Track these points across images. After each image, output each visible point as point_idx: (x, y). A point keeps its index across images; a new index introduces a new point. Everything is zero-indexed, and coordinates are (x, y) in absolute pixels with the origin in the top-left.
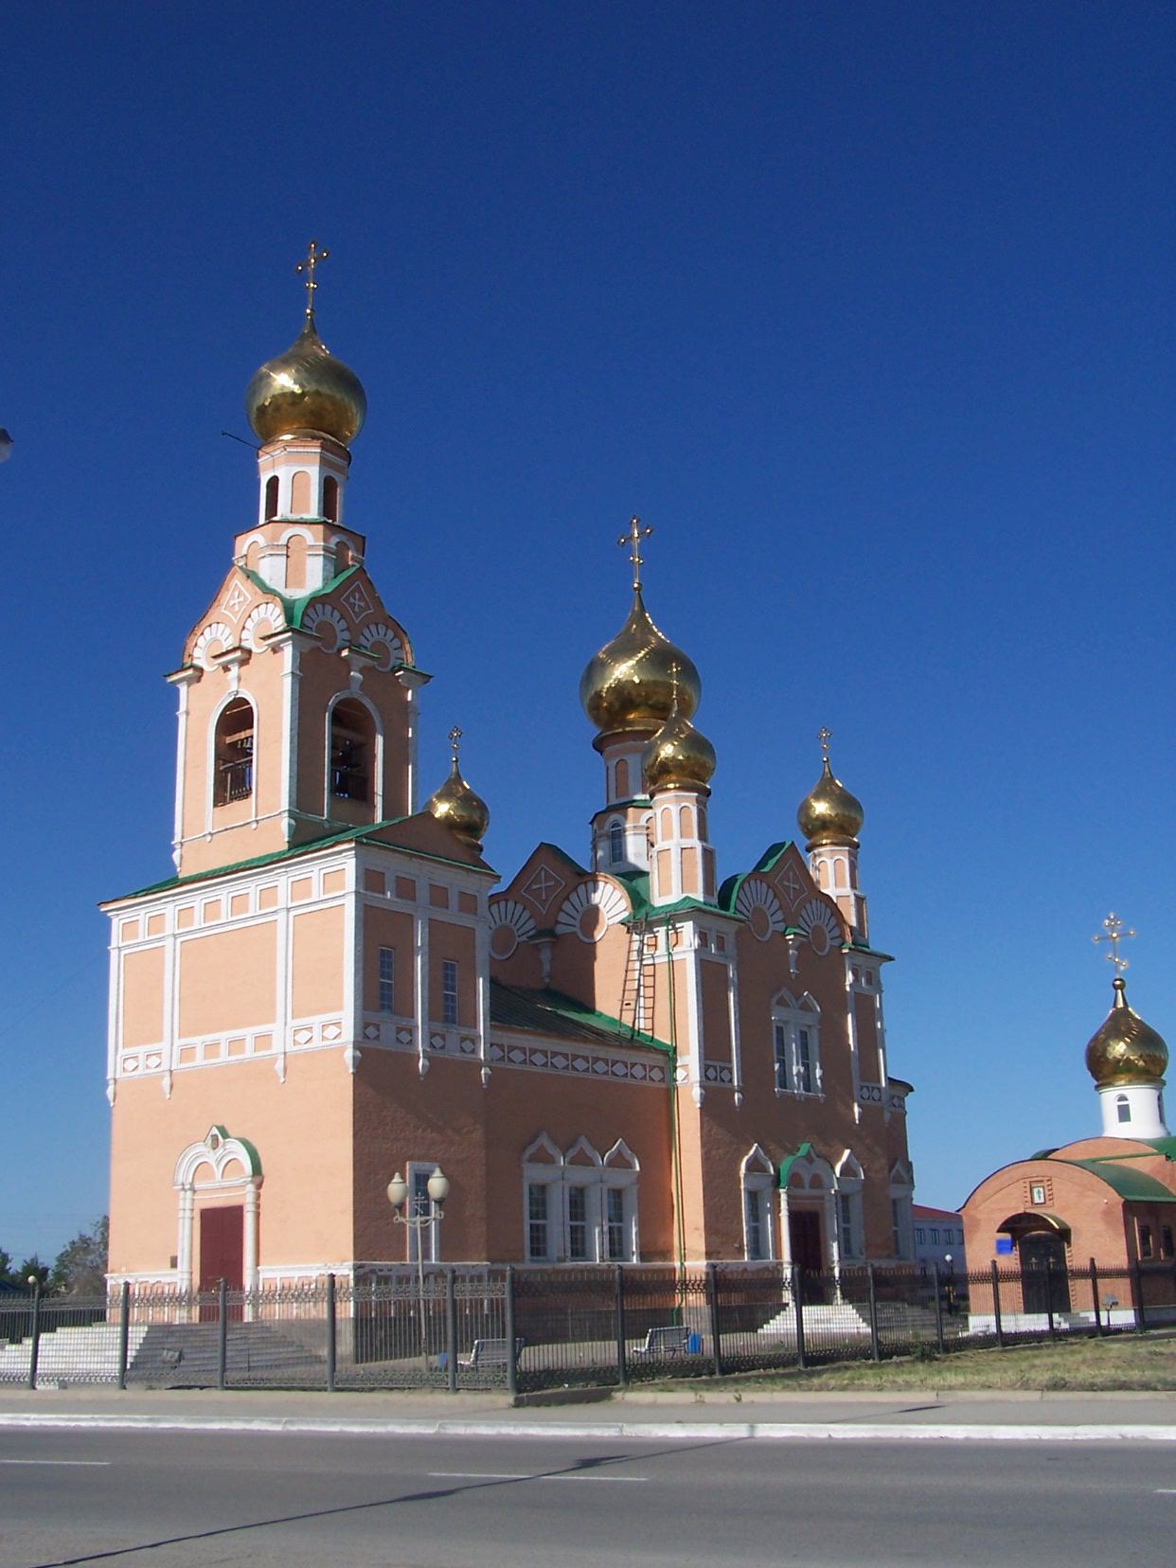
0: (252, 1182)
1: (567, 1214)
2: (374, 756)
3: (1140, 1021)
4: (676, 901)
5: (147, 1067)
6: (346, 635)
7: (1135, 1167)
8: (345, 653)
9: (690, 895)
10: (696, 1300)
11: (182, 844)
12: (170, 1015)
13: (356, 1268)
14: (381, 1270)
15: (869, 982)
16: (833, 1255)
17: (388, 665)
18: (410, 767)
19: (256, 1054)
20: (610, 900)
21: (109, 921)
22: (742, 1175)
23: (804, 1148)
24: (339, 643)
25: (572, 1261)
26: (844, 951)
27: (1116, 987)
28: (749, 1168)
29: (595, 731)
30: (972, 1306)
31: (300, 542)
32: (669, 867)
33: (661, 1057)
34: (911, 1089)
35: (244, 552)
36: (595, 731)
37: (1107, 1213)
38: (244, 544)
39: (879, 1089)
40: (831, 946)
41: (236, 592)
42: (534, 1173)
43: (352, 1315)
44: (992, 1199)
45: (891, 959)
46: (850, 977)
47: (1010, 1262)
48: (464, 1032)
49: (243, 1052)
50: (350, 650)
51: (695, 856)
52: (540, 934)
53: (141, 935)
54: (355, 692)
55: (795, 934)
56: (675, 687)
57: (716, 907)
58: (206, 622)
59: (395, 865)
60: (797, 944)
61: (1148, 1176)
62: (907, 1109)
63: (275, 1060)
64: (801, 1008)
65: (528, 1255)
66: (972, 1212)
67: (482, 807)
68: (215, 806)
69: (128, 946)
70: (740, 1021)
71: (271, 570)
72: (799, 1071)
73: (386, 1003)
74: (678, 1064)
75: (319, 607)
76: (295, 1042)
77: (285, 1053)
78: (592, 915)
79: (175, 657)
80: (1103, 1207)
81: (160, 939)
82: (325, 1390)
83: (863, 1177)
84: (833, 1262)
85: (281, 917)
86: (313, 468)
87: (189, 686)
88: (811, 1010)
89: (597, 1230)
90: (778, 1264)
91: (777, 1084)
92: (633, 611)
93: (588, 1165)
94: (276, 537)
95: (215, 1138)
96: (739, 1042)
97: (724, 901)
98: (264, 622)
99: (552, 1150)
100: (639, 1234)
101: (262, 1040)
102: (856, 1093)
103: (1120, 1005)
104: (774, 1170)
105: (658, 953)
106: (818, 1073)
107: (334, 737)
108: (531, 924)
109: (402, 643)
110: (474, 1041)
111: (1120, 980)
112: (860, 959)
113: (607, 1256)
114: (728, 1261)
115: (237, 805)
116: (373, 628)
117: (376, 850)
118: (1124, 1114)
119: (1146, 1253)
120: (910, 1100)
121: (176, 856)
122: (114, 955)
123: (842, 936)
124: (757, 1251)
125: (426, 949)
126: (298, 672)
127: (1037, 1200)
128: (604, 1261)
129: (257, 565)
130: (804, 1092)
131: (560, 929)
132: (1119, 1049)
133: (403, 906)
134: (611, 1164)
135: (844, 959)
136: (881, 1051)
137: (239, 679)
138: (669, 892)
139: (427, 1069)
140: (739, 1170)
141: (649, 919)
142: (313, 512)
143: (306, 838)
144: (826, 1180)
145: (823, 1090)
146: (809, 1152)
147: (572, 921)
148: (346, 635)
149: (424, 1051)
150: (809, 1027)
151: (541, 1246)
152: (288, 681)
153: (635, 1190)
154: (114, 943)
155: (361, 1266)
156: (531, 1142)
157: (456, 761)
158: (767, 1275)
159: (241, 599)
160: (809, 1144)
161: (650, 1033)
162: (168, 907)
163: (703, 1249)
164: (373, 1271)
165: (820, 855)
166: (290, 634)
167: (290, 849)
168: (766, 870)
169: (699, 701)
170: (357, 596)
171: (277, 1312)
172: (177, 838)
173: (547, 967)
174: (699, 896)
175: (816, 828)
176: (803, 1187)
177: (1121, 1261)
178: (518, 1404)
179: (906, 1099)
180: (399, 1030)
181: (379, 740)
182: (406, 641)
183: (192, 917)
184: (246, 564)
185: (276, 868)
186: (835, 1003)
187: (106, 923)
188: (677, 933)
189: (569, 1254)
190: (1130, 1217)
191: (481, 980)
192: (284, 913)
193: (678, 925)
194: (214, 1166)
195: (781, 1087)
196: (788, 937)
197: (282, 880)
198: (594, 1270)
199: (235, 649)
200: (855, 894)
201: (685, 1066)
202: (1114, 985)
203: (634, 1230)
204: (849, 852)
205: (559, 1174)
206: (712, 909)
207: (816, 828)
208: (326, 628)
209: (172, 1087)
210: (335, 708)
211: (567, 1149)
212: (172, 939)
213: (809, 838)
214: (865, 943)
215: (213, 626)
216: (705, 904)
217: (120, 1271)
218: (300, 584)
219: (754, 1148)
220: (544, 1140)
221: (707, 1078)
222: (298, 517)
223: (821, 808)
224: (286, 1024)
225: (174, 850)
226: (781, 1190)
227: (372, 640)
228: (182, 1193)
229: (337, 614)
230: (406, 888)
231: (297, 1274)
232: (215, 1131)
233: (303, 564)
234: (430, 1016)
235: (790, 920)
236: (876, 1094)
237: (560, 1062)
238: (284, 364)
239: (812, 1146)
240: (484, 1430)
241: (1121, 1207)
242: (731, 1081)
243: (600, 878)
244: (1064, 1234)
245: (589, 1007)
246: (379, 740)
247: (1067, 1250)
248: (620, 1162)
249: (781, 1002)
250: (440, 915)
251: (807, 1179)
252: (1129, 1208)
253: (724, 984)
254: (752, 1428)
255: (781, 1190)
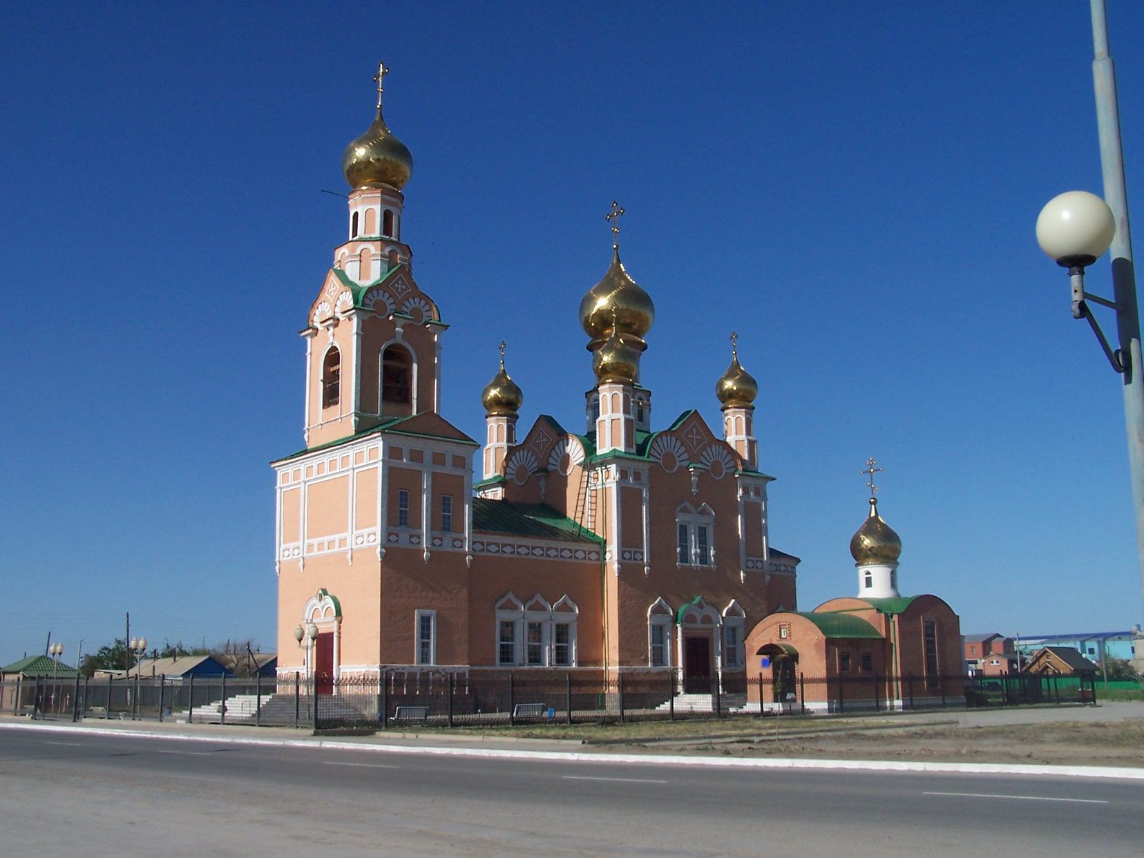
0: (336, 620)
1: (526, 638)
2: (411, 376)
3: (884, 524)
4: (607, 452)
5: (369, 542)
6: (393, 307)
7: (859, 616)
8: (391, 318)
9: (617, 448)
10: (614, 690)
11: (308, 429)
12: (303, 528)
13: (381, 668)
14: (397, 669)
15: (757, 493)
16: (717, 664)
17: (422, 320)
18: (436, 381)
19: (340, 549)
20: (575, 450)
21: (276, 472)
22: (648, 616)
23: (698, 599)
24: (388, 311)
25: (529, 665)
26: (737, 476)
27: (871, 503)
28: (653, 612)
29: (589, 339)
30: (749, 698)
31: (368, 253)
32: (604, 433)
33: (597, 546)
34: (799, 561)
35: (339, 259)
36: (589, 339)
37: (817, 645)
38: (342, 252)
39: (762, 562)
40: (726, 473)
41: (333, 282)
42: (503, 616)
43: (379, 693)
44: (761, 634)
45: (774, 479)
46: (740, 492)
47: (768, 673)
48: (455, 536)
49: (323, 550)
50: (394, 316)
51: (620, 423)
52: (539, 471)
53: (338, 469)
54: (399, 340)
55: (694, 468)
56: (614, 319)
57: (634, 454)
58: (319, 301)
59: (407, 443)
60: (698, 473)
61: (865, 622)
62: (797, 574)
63: (347, 553)
64: (699, 513)
65: (498, 661)
66: (751, 642)
67: (518, 391)
68: (324, 408)
69: (311, 480)
70: (650, 524)
71: (352, 271)
72: (696, 552)
73: (403, 521)
74: (607, 550)
75: (375, 292)
76: (356, 544)
77: (352, 549)
78: (566, 458)
79: (305, 323)
80: (815, 641)
81: (299, 483)
82: (254, 725)
83: (745, 616)
84: (718, 668)
85: (302, 485)
86: (377, 206)
87: (312, 338)
88: (709, 514)
89: (547, 648)
90: (674, 669)
91: (678, 560)
92: (613, 263)
93: (515, 609)
94: (353, 250)
95: (320, 595)
96: (649, 536)
97: (641, 450)
98: (344, 302)
99: (543, 602)
100: (578, 650)
101: (342, 542)
102: (742, 568)
103: (873, 514)
104: (673, 613)
105: (598, 483)
106: (712, 552)
107: (385, 368)
108: (535, 465)
109: (431, 306)
110: (462, 541)
111: (874, 499)
112: (748, 481)
113: (554, 662)
114: (635, 667)
115: (332, 408)
116: (411, 301)
117: (395, 436)
118: (869, 583)
119: (843, 668)
120: (798, 568)
121: (306, 436)
122: (278, 491)
123: (736, 466)
124: (659, 658)
125: (430, 490)
126: (361, 333)
127: (783, 636)
128: (551, 666)
129: (345, 267)
130: (700, 565)
131: (550, 468)
132: (867, 542)
133: (416, 466)
134: (558, 609)
135: (737, 482)
136: (764, 538)
137: (334, 335)
138: (604, 446)
139: (428, 558)
140: (647, 612)
141: (592, 463)
142: (377, 233)
143: (363, 429)
144: (714, 619)
145: (716, 563)
146: (700, 602)
147: (707, 463)
148: (393, 307)
149: (427, 548)
150: (708, 524)
151: (509, 656)
152: (355, 337)
153: (575, 624)
154: (278, 486)
155: (384, 667)
156: (503, 596)
157: (503, 363)
158: (665, 677)
159: (335, 288)
160: (700, 597)
161: (593, 531)
162: (301, 465)
163: (618, 660)
164: (393, 670)
165: (727, 415)
166: (354, 311)
167: (356, 434)
168: (674, 429)
169: (654, 320)
170: (400, 282)
171: (348, 690)
172: (307, 426)
173: (543, 491)
174: (622, 448)
175: (726, 397)
176: (696, 622)
177: (822, 673)
178: (316, 734)
179: (797, 567)
180: (411, 536)
181: (415, 366)
182: (433, 306)
183: (323, 468)
184: (340, 266)
185: (348, 446)
186: (727, 508)
187: (274, 474)
188: (608, 471)
189: (527, 661)
190: (831, 647)
191: (467, 506)
192: (351, 471)
193: (608, 466)
194: (321, 609)
195: (681, 562)
196: (690, 470)
197: (350, 451)
198: (431, 667)
199: (330, 319)
200: (748, 439)
201: (610, 551)
202: (870, 502)
203: (574, 648)
204: (746, 413)
205: (521, 615)
206: (633, 457)
207: (726, 397)
208: (380, 306)
209: (304, 566)
210: (385, 350)
211: (526, 602)
212: (352, 470)
213: (723, 402)
214: (755, 470)
215: (323, 303)
216: (625, 453)
217: (282, 666)
218: (368, 278)
219: (658, 600)
220: (510, 596)
221: (624, 558)
222: (368, 237)
223: (729, 384)
224: (352, 533)
225: (305, 433)
226: (678, 625)
227: (410, 307)
228: (307, 625)
229: (387, 295)
230: (416, 456)
231: (356, 670)
232: (320, 592)
233: (369, 265)
234: (433, 527)
235: (692, 459)
236: (759, 565)
237: (523, 551)
238: (360, 144)
239: (702, 598)
240: (300, 744)
241: (824, 641)
242: (642, 559)
243: (570, 437)
244: (794, 657)
245: (561, 514)
246: (415, 366)
247: (796, 666)
248: (565, 608)
249: (685, 510)
250: (439, 470)
251: (699, 618)
252: (830, 643)
253: (640, 501)
254: (321, 743)
255: (678, 625)
